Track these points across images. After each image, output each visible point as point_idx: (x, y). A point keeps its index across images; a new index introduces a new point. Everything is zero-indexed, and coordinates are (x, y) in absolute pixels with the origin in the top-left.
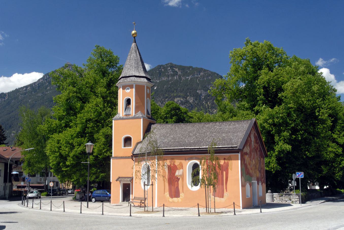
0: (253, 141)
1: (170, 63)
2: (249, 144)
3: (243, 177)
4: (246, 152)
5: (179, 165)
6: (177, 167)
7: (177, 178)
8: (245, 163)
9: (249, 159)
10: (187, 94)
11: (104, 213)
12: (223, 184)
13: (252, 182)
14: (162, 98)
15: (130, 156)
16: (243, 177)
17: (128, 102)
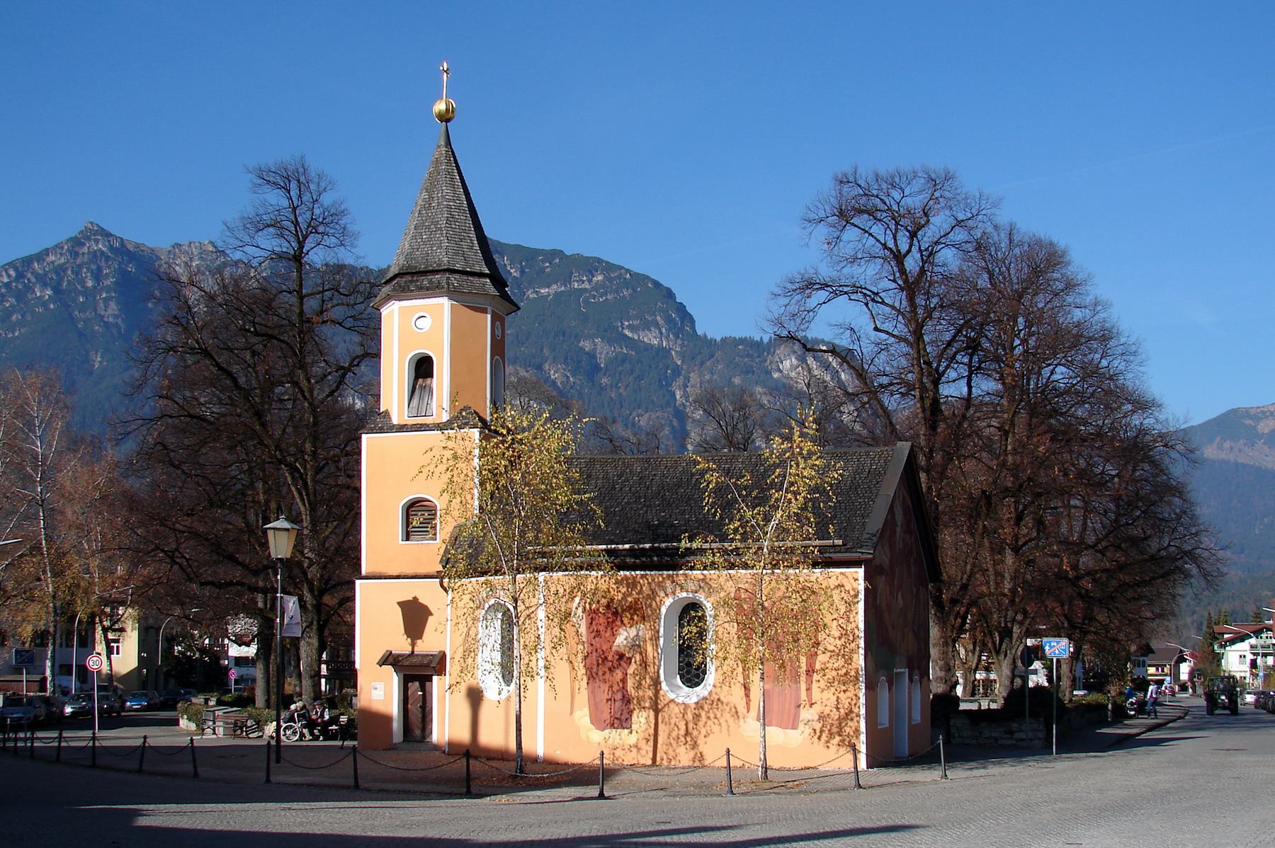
0: (899, 524)
4: (881, 564)
10: (542, 350)
17: (423, 367)
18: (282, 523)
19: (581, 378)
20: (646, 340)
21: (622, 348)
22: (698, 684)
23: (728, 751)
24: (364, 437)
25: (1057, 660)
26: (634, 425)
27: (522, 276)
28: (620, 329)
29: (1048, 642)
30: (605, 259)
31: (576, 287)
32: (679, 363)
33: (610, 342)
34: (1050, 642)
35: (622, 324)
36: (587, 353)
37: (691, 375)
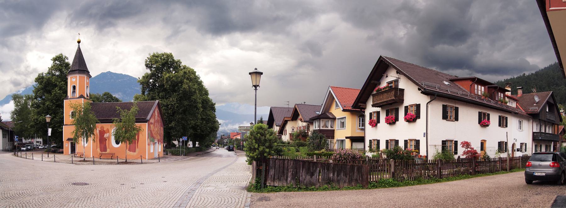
2: (154, 117)
12: (136, 143)
17: (74, 87)
18: (48, 116)
23: (117, 157)
24: (64, 100)
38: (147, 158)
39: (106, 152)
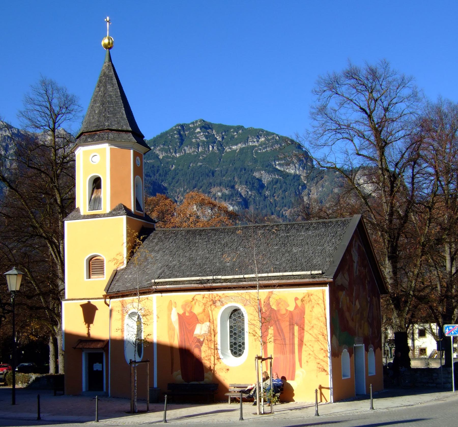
0: (356, 261)
1: (200, 121)
2: (347, 267)
3: (336, 335)
4: (342, 285)
5: (202, 313)
6: (198, 316)
7: (199, 341)
8: (340, 307)
9: (348, 298)
10: (234, 178)
11: (42, 415)
12: (293, 352)
13: (354, 345)
14: (185, 187)
15: (102, 297)
16: (334, 336)
19: (255, 192)
20: (287, 171)
21: (275, 176)
22: (240, 355)
25: (453, 337)
26: (283, 215)
27: (222, 140)
28: (274, 166)
29: (447, 327)
30: (266, 129)
31: (251, 144)
32: (305, 182)
33: (269, 172)
34: (448, 327)
35: (275, 163)
36: (258, 179)
37: (312, 188)
38: (148, 399)
39: (202, 382)
